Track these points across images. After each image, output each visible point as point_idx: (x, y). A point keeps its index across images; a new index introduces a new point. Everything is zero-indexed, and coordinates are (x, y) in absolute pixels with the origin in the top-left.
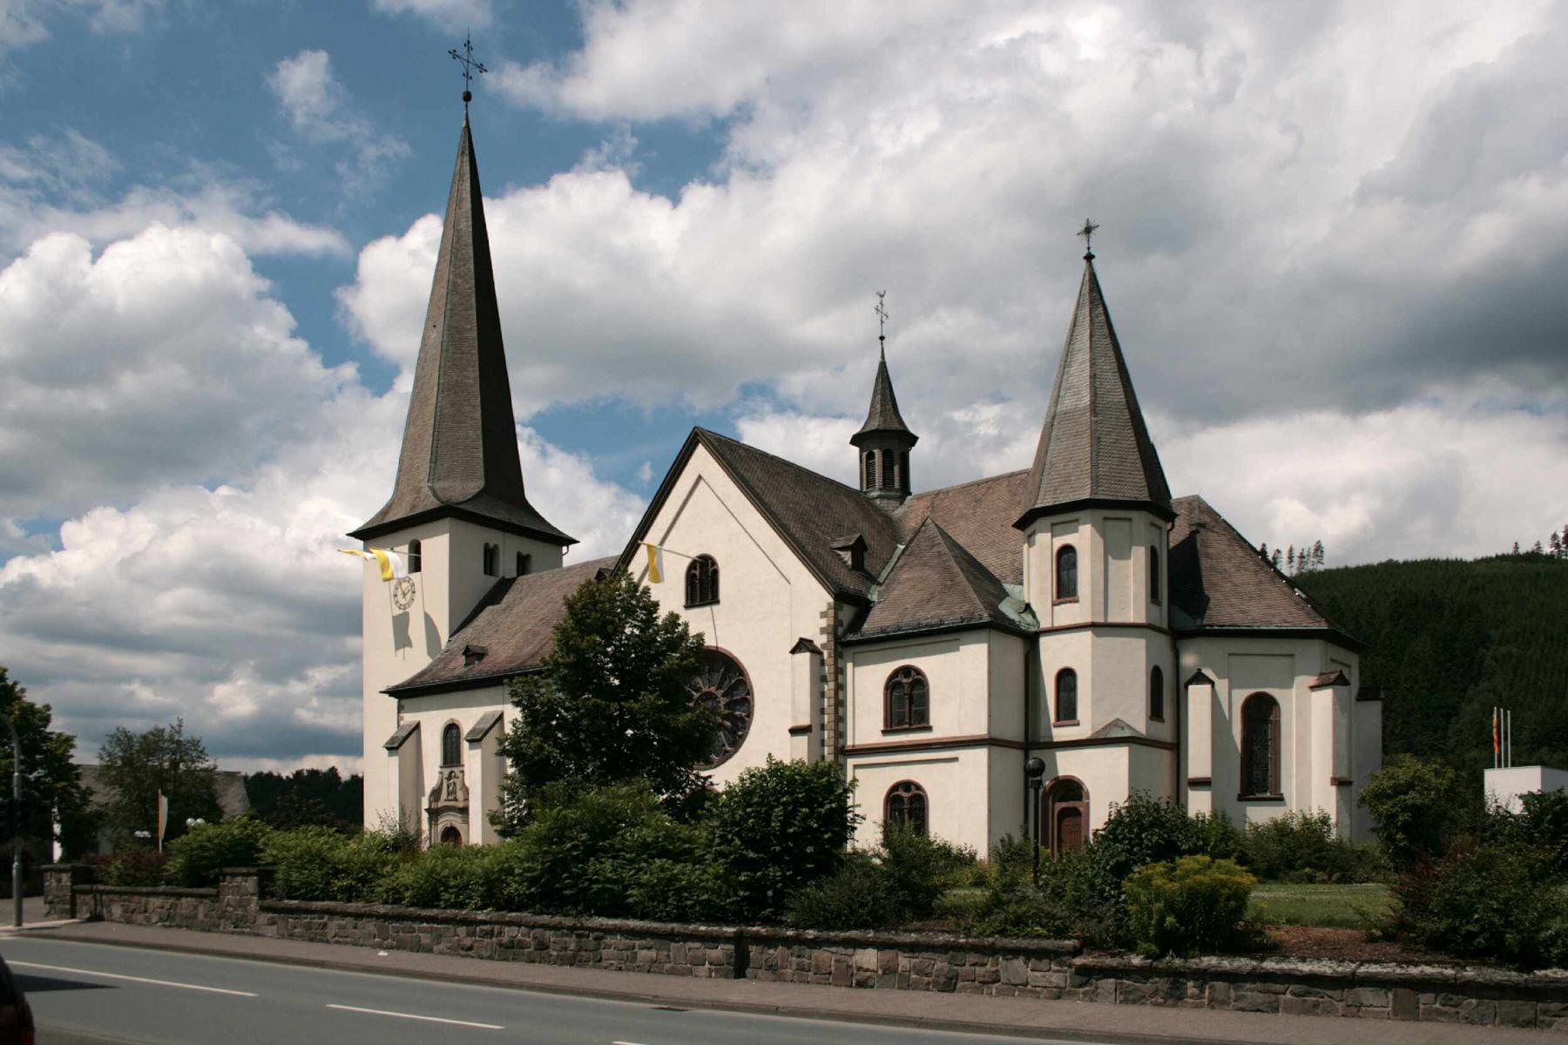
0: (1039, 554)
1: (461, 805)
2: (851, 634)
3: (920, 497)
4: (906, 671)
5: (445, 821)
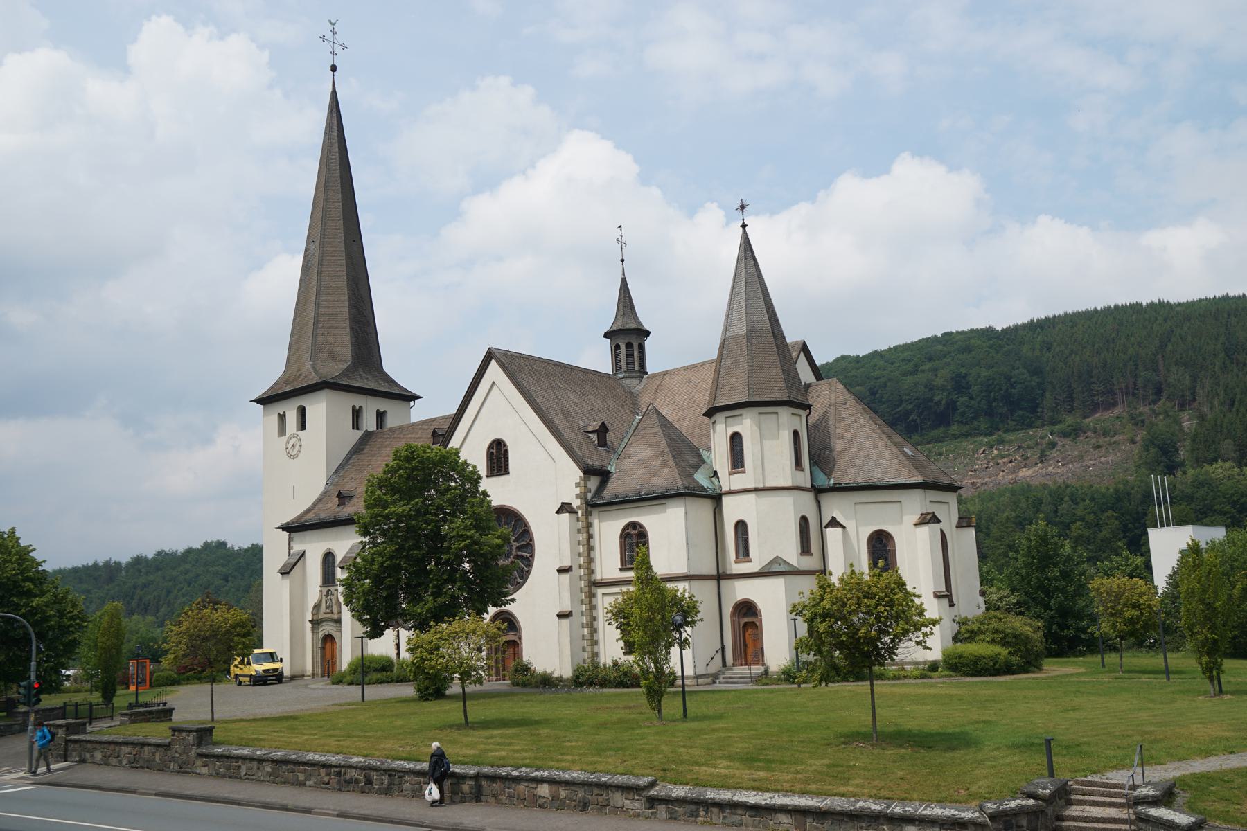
0: (720, 434)
1: (335, 617)
2: (599, 495)
4: (634, 525)
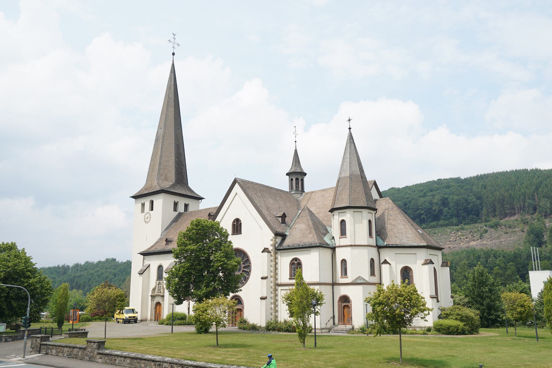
0: (336, 219)
1: (162, 294)
2: (280, 247)
3: (307, 193)
5: (158, 299)
